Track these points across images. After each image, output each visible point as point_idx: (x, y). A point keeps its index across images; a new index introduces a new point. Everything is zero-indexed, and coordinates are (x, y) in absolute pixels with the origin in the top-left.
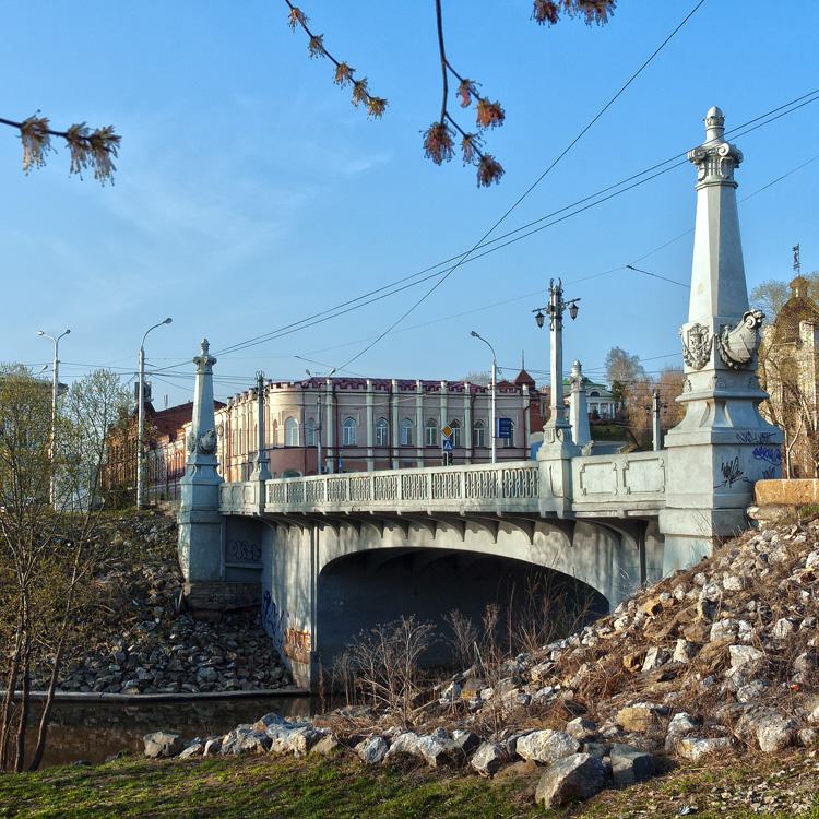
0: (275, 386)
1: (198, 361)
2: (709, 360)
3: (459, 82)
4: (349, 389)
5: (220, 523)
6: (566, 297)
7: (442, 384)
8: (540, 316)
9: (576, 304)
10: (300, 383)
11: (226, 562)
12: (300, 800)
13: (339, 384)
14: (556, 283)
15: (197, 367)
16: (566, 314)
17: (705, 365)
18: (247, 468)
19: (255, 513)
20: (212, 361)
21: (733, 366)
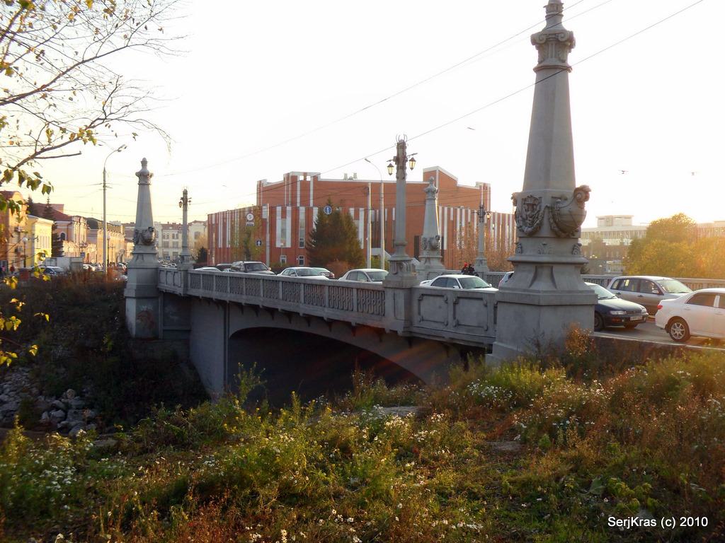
6: (409, 151)
9: (414, 156)
16: (408, 164)
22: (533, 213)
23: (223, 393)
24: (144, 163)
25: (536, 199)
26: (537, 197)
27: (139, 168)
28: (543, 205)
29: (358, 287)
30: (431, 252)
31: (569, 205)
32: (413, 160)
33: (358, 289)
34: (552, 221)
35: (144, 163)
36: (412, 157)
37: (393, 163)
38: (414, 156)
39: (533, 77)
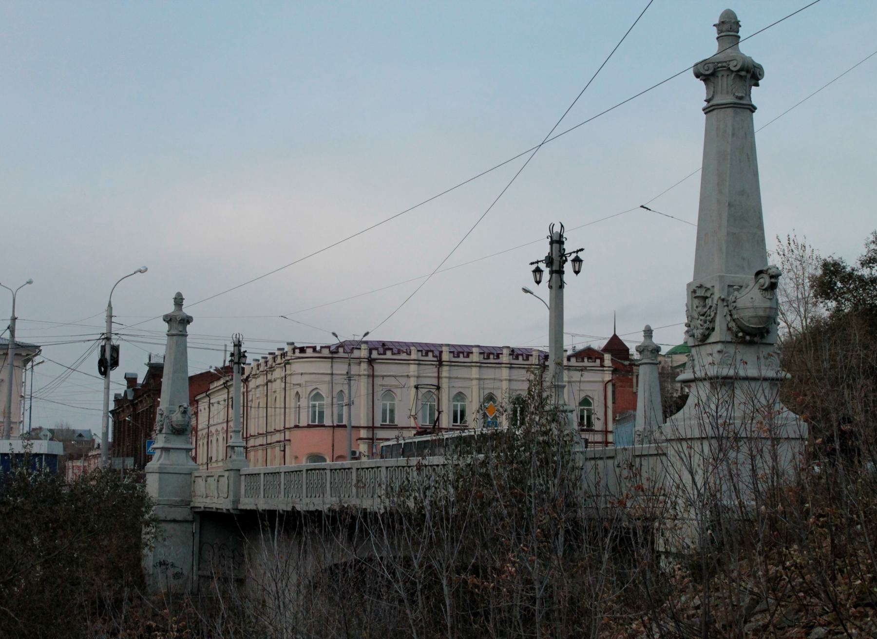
0: (297, 351)
1: (168, 319)
2: (713, 329)
3: (11, 315)
4: (389, 354)
5: (192, 522)
6: (568, 247)
7: (505, 351)
8: (538, 271)
9: (580, 254)
10: (329, 347)
11: (199, 569)
12: (50, 557)
13: (376, 349)
14: (557, 229)
15: (166, 326)
16: (568, 267)
17: (709, 335)
18: (767, 592)
19: (228, 510)
20: (187, 320)
21: (743, 337)
22: (705, 310)
23: (341, 540)
24: (179, 301)
25: (707, 289)
26: (709, 286)
27: (170, 308)
28: (716, 297)
29: (332, 468)
30: (173, 437)
31: (773, 482)
32: (577, 260)
33: (331, 470)
34: (729, 318)
35: (179, 301)
36: (573, 256)
37: (542, 266)
38: (580, 254)
39: (739, 19)
